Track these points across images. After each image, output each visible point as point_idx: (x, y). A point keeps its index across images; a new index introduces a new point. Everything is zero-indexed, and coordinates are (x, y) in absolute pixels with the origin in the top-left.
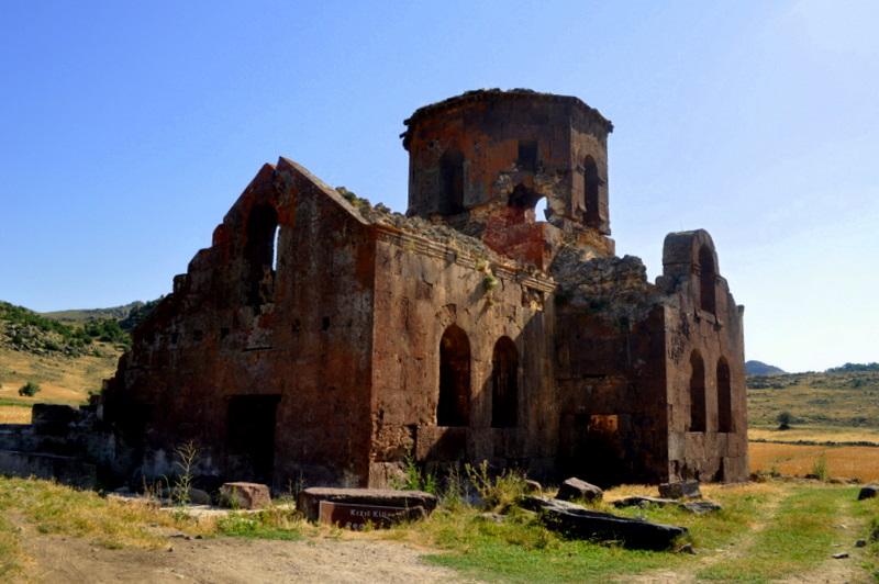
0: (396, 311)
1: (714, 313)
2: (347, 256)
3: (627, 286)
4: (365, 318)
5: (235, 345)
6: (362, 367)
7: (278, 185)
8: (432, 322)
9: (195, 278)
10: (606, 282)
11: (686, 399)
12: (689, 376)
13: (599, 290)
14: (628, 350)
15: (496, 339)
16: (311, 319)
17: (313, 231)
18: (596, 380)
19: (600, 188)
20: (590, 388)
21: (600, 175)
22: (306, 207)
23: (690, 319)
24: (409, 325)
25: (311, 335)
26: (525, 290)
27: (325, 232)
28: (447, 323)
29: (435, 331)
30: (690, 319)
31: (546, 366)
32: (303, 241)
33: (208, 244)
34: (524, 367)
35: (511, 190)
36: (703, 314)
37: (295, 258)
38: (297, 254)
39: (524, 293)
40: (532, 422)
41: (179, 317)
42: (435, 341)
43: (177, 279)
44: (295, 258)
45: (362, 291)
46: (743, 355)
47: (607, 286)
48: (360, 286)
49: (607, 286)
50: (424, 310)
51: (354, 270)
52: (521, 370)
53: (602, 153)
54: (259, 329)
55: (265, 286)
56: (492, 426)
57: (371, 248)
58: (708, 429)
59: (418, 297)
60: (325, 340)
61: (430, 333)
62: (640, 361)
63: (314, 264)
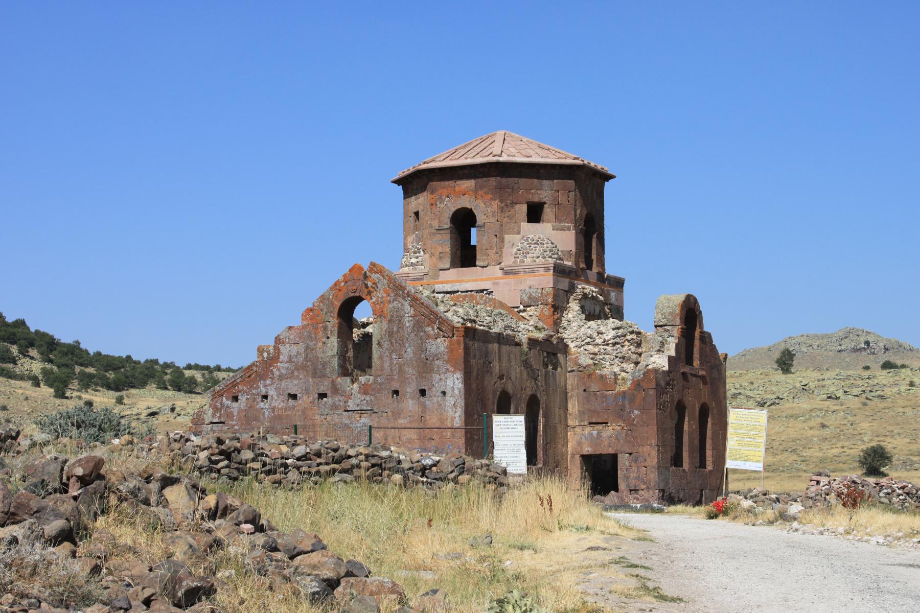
5: (335, 407)
7: (370, 284)
9: (285, 350)
12: (463, 441)
14: (627, 403)
16: (408, 390)
17: (407, 325)
18: (600, 427)
22: (399, 305)
25: (410, 401)
27: (418, 326)
32: (398, 332)
35: (495, 330)
37: (392, 344)
38: (393, 341)
41: (268, 382)
43: (21, 323)
44: (392, 344)
46: (526, 422)
48: (451, 369)
51: (446, 357)
60: (424, 407)
61: (490, 396)
62: (636, 412)
63: (409, 350)
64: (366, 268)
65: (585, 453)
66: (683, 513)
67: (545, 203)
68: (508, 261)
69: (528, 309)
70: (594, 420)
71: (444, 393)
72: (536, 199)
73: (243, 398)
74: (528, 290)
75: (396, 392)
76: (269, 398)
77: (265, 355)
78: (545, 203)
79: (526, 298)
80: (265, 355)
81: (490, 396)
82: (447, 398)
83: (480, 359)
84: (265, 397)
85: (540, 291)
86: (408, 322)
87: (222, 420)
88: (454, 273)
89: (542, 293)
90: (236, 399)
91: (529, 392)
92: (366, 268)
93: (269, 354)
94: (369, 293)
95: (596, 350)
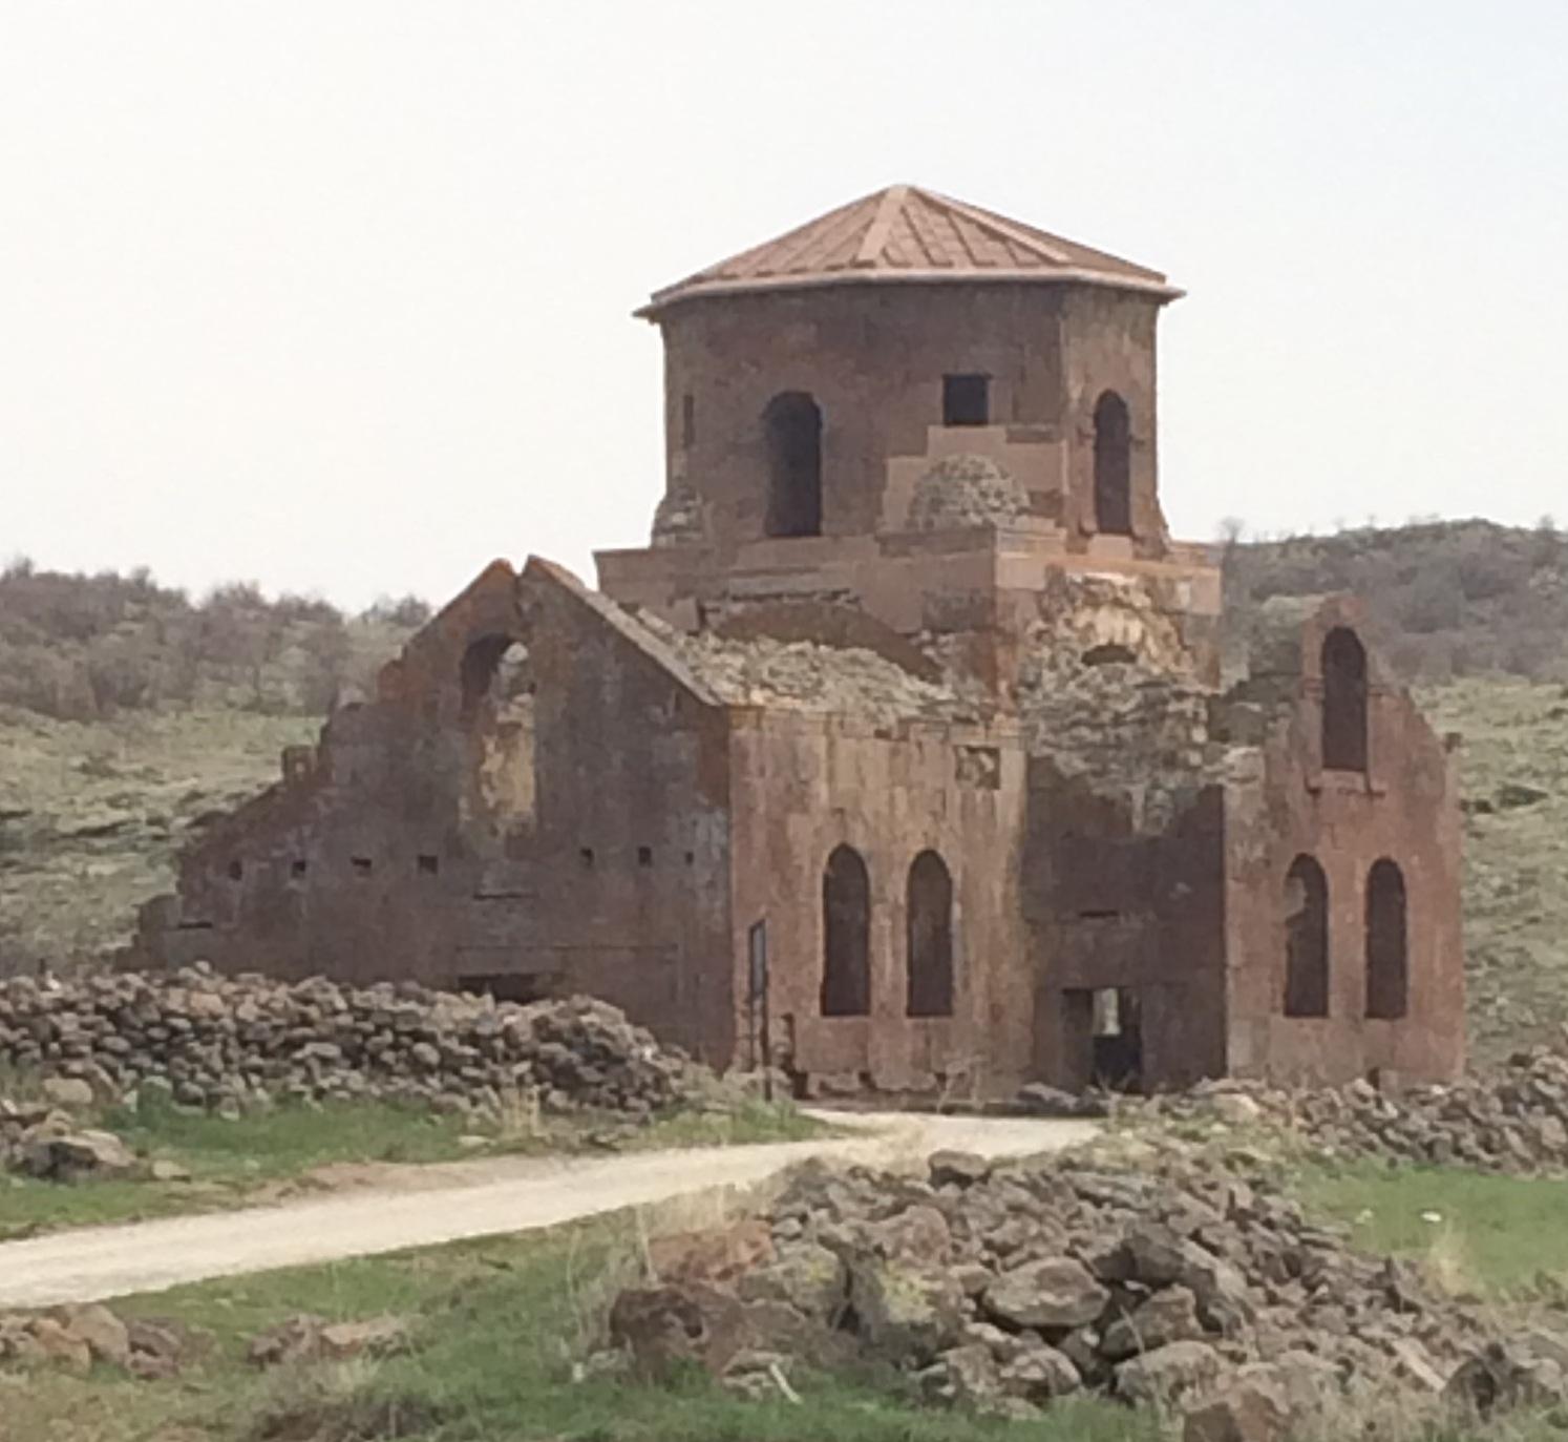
0: (759, 838)
1: (1363, 769)
2: (683, 747)
3: (1166, 731)
4: (716, 854)
6: (720, 929)
7: (526, 606)
8: (811, 843)
9: (339, 755)
10: (1124, 724)
11: (747, 966)
13: (1112, 740)
15: (911, 858)
19: (1134, 455)
20: (1089, 937)
21: (1134, 429)
23: (1296, 796)
24: (780, 854)
26: (964, 754)
28: (835, 843)
29: (814, 862)
30: (1296, 796)
31: (1005, 896)
33: (197, 597)
34: (962, 903)
36: (1329, 779)
39: (960, 761)
40: (980, 1004)
41: (307, 831)
42: (813, 876)
45: (710, 810)
47: (1126, 732)
48: (705, 801)
49: (1126, 732)
50: (799, 828)
52: (957, 910)
53: (1138, 370)
54: (506, 862)
55: (489, 774)
56: (910, 1013)
57: (723, 744)
58: (1334, 1011)
59: (788, 809)
62: (1182, 887)
64: (518, 567)
65: (1070, 985)
66: (151, 1277)
67: (989, 377)
68: (892, 520)
69: (942, 639)
70: (1095, 907)
71: (690, 858)
72: (966, 369)
73: (250, 868)
74: (939, 593)
75: (588, 853)
76: (309, 869)
77: (300, 768)
78: (989, 377)
79: (934, 613)
80: (300, 768)
81: (806, 863)
82: (696, 865)
83: (776, 774)
84: (300, 866)
85: (966, 596)
86: (609, 696)
87: (208, 918)
88: (769, 552)
89: (972, 600)
90: (236, 871)
91: (918, 847)
92: (518, 567)
93: (308, 767)
94: (526, 627)
95: (1097, 737)
